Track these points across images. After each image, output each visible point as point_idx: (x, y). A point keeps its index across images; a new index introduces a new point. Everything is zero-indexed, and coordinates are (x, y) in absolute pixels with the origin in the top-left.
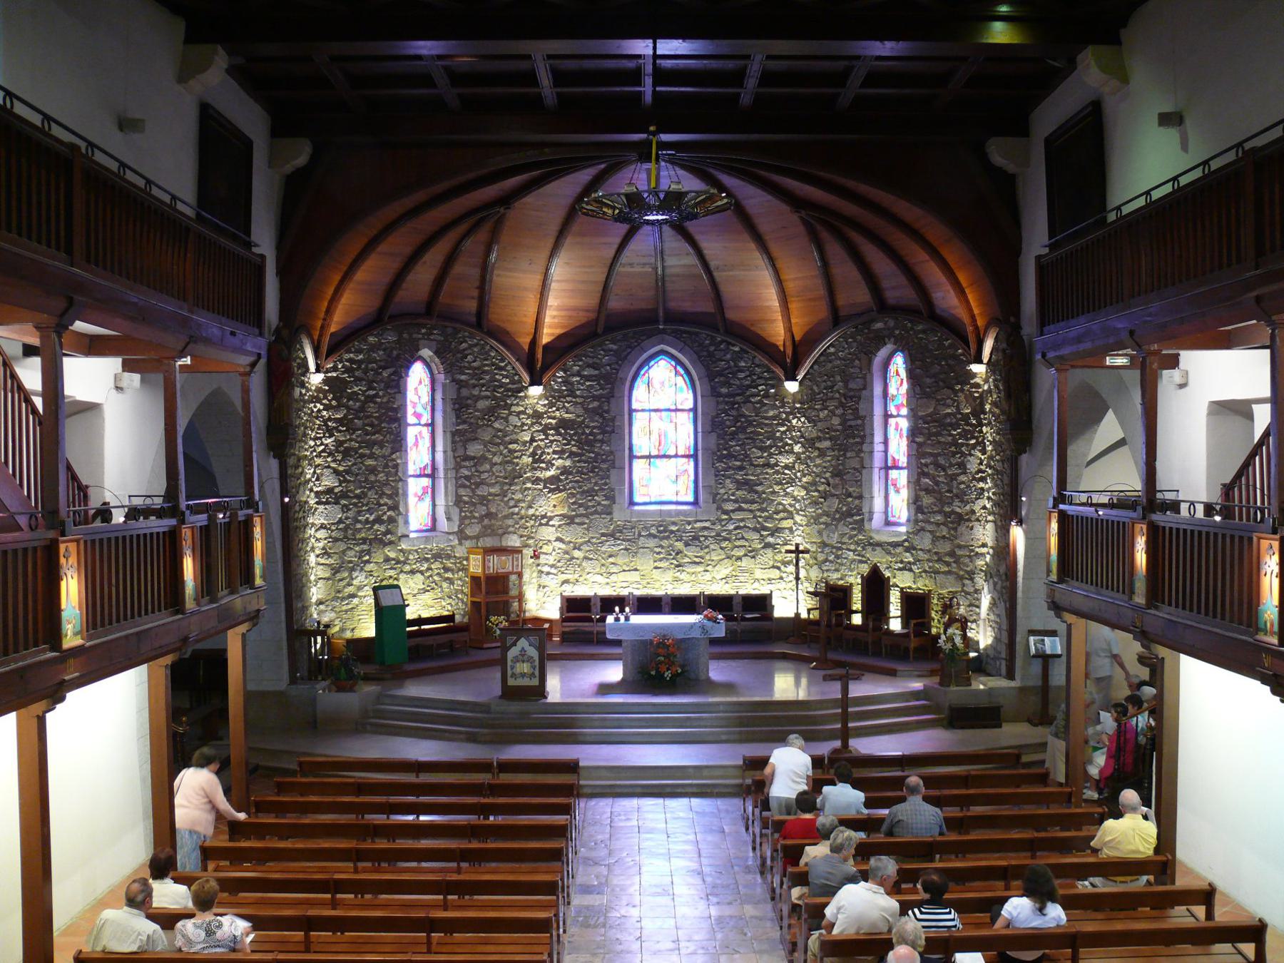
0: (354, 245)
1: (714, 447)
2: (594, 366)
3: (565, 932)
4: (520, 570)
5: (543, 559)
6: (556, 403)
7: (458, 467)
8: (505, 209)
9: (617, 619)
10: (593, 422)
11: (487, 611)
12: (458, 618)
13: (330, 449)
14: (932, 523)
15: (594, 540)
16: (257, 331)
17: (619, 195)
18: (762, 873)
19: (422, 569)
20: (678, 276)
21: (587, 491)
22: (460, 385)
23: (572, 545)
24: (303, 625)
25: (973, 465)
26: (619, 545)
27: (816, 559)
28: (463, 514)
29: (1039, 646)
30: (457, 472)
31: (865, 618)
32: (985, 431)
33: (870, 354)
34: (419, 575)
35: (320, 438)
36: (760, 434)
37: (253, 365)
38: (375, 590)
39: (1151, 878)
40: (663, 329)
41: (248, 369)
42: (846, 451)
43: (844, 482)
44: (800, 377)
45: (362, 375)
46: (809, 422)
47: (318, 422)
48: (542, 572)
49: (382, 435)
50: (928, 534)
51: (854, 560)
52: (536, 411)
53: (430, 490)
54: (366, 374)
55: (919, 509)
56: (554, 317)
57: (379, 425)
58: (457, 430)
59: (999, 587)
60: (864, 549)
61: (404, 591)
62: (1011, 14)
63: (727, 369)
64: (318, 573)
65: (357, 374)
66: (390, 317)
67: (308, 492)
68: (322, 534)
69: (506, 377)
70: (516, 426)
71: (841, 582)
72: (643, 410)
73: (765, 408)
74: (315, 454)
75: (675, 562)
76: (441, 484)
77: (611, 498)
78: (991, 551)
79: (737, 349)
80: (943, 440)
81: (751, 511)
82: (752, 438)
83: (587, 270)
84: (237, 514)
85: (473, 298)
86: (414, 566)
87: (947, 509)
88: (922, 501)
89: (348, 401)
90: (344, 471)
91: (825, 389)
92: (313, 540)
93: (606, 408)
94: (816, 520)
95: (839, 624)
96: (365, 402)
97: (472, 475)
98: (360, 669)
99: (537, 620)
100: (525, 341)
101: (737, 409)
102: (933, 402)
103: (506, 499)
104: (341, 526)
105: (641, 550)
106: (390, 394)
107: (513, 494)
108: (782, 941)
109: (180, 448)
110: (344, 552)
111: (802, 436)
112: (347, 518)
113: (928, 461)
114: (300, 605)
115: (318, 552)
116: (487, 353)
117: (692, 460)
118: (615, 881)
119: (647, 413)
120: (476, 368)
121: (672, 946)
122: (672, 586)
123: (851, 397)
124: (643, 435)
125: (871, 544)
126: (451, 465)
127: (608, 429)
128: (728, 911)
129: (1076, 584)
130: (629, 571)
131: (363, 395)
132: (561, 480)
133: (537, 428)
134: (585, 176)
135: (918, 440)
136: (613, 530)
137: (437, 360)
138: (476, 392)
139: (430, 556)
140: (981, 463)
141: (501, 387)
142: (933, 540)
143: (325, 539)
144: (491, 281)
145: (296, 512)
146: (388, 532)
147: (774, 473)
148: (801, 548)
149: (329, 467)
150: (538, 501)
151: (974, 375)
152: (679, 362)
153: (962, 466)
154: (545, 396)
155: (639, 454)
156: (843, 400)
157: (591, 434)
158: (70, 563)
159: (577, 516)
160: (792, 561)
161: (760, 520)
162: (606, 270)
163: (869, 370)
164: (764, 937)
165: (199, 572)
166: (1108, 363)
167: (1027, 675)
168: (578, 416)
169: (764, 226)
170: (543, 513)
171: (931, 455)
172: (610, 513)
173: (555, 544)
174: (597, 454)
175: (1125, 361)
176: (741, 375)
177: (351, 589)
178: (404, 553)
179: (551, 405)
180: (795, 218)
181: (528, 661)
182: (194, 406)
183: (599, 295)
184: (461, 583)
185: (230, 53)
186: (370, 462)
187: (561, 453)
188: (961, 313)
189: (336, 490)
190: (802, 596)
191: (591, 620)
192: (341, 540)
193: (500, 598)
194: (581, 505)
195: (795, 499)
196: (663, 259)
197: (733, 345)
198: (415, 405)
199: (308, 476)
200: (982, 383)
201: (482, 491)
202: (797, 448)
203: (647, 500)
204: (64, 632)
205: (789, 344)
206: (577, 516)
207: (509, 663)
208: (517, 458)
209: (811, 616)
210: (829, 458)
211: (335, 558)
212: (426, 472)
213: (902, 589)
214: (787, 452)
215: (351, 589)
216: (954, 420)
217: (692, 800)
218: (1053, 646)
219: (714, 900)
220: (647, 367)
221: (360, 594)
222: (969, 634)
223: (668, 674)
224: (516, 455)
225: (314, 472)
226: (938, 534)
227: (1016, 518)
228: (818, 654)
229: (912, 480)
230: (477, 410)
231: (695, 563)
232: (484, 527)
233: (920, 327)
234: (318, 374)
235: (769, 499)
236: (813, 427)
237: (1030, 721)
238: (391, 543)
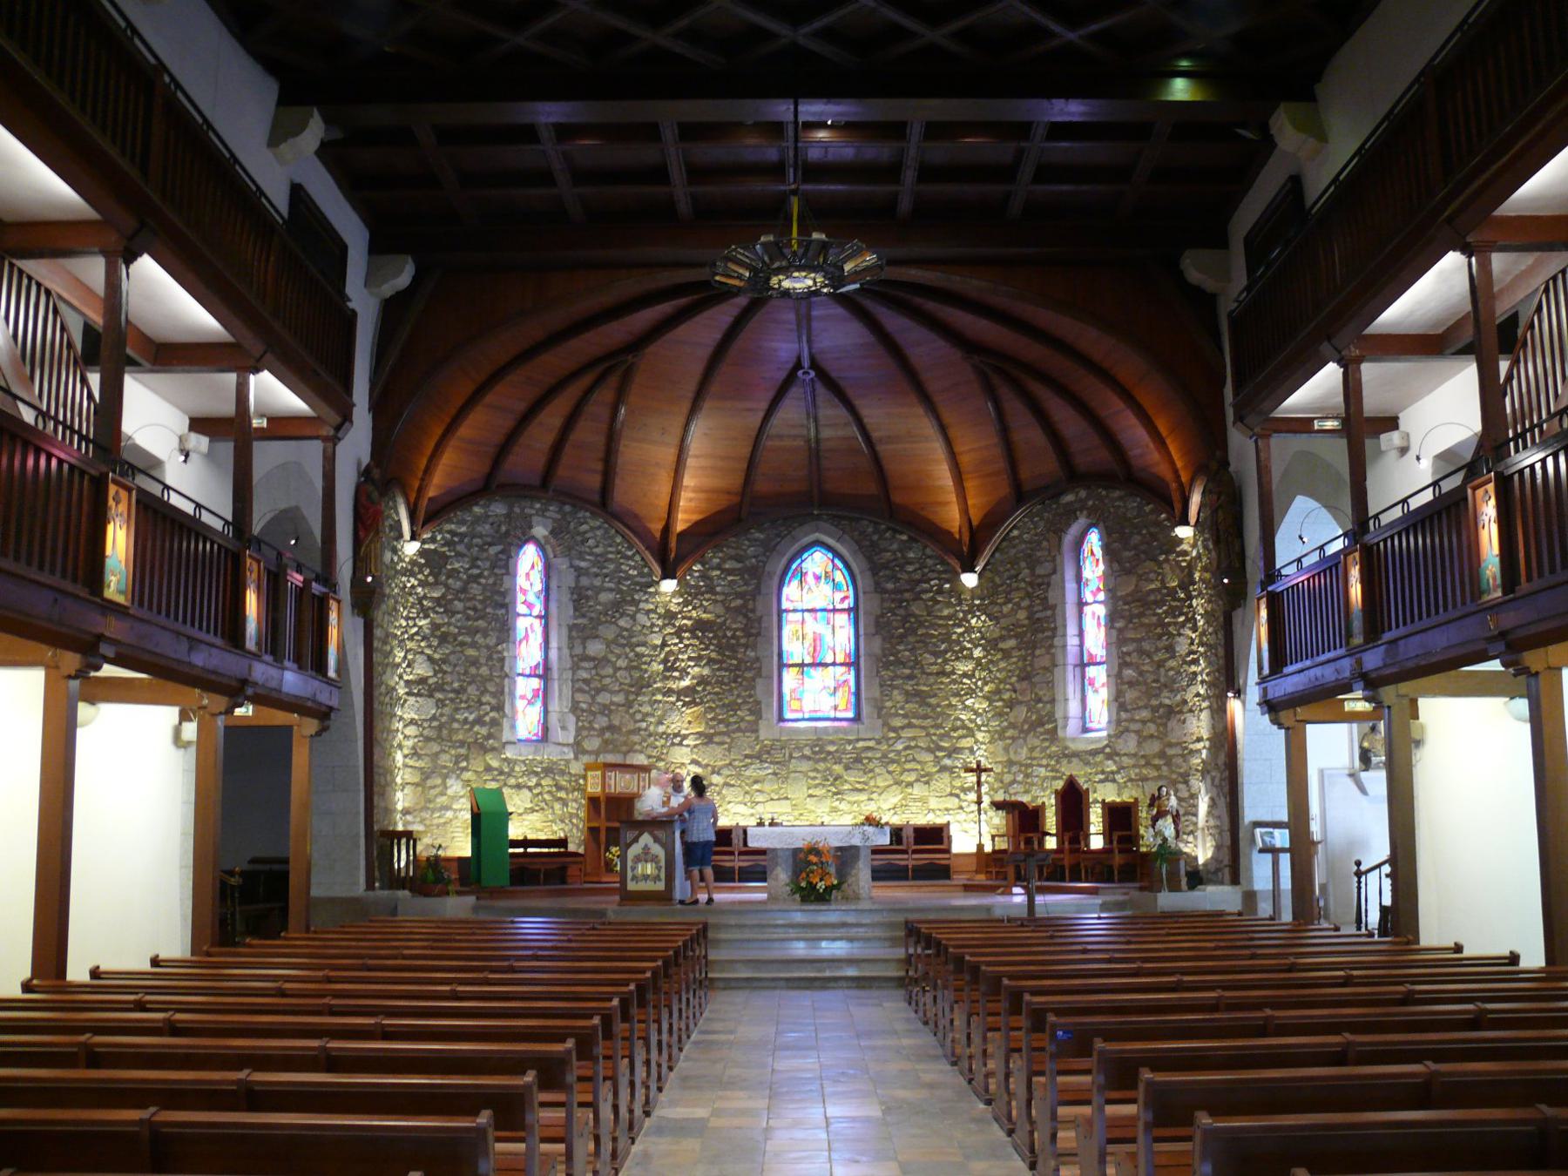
1: (878, 651)
2: (738, 559)
7: (575, 668)
8: (634, 357)
10: (735, 622)
14: (1137, 721)
15: (736, 763)
19: (530, 784)
21: (729, 705)
22: (580, 572)
25: (1182, 647)
27: (1002, 782)
28: (580, 724)
29: (1267, 839)
30: (573, 674)
31: (1060, 842)
32: (1195, 605)
33: (1059, 532)
34: (526, 792)
35: (414, 619)
36: (933, 636)
42: (1035, 648)
44: (978, 569)
46: (991, 620)
50: (1133, 735)
51: (1047, 777)
52: (668, 611)
54: (469, 550)
56: (691, 500)
60: (1058, 762)
62: (1196, 69)
64: (406, 777)
66: (498, 486)
68: (412, 730)
72: (795, 611)
75: (834, 790)
77: (757, 712)
79: (904, 537)
80: (1147, 621)
82: (924, 641)
86: (520, 780)
87: (1154, 702)
89: (448, 578)
90: (440, 659)
91: (1008, 579)
94: (1000, 735)
96: (467, 583)
97: (592, 678)
100: (656, 527)
103: (631, 711)
104: (435, 724)
105: (793, 775)
106: (496, 575)
110: (437, 755)
111: (982, 638)
112: (442, 715)
115: (406, 751)
116: (612, 538)
117: (852, 668)
123: (1039, 585)
130: (779, 799)
133: (669, 630)
135: (1118, 625)
136: (760, 752)
138: (597, 582)
139: (539, 770)
140: (1192, 644)
141: (627, 579)
143: (416, 737)
145: (381, 694)
146: (490, 736)
147: (950, 683)
149: (422, 653)
151: (1181, 541)
152: (837, 554)
153: (1170, 649)
156: (1030, 589)
157: (733, 637)
158: (120, 510)
160: (973, 787)
161: (934, 738)
163: (1059, 551)
166: (1316, 427)
168: (719, 617)
169: (933, 386)
170: (676, 731)
171: (1133, 640)
172: (756, 731)
174: (740, 661)
175: (1336, 423)
176: (910, 568)
177: (442, 800)
178: (509, 764)
179: (686, 603)
184: (576, 807)
185: (327, 120)
186: (471, 652)
187: (698, 659)
188: (1163, 470)
189: (431, 681)
192: (434, 740)
194: (721, 722)
195: (976, 713)
197: (901, 533)
198: (524, 592)
199: (398, 660)
201: (604, 698)
202: (977, 653)
203: (799, 716)
204: (107, 582)
207: (629, 864)
208: (645, 663)
210: (1014, 660)
214: (965, 657)
215: (442, 800)
216: (1159, 597)
221: (455, 807)
223: (821, 886)
224: (644, 659)
225: (405, 657)
226: (1145, 734)
230: (599, 604)
235: (945, 713)
238: (493, 749)
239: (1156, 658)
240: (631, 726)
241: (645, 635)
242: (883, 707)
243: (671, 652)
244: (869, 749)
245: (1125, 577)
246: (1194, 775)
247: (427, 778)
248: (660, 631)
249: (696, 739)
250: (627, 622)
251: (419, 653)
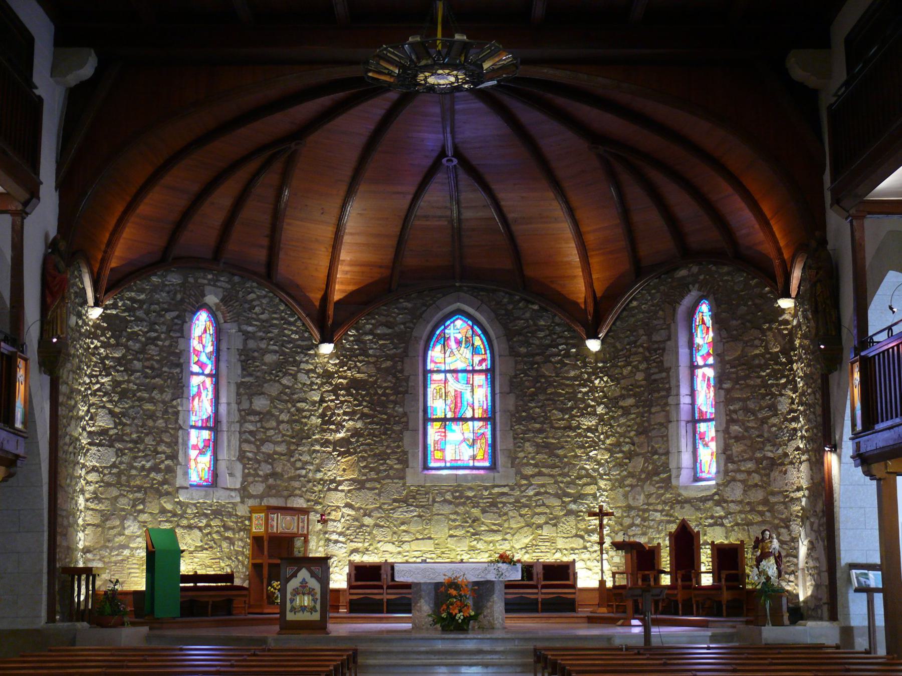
2: (388, 325)
4: (305, 532)
5: (331, 526)
6: (347, 363)
7: (242, 421)
10: (385, 381)
13: (106, 388)
15: (386, 506)
19: (200, 525)
21: (379, 455)
22: (247, 336)
23: (362, 511)
25: (784, 405)
26: (411, 511)
28: (246, 471)
30: (241, 426)
32: (795, 368)
33: (674, 303)
34: (197, 532)
35: (96, 376)
36: (561, 395)
40: (460, 287)
42: (651, 406)
45: (144, 316)
46: (612, 381)
47: (95, 359)
48: (330, 540)
49: (162, 379)
50: (739, 484)
51: (662, 521)
52: (326, 371)
55: (729, 459)
56: (347, 272)
58: (243, 382)
59: (815, 526)
60: (672, 508)
63: (526, 327)
67: (80, 430)
69: (296, 332)
70: (305, 384)
73: (566, 368)
74: (89, 392)
75: (472, 531)
79: (536, 307)
86: (192, 521)
87: (758, 455)
88: (731, 450)
89: (128, 341)
90: (120, 413)
91: (628, 344)
92: (83, 482)
93: (399, 368)
94: (619, 483)
96: (145, 345)
103: (292, 460)
104: (115, 471)
105: (436, 517)
106: (172, 338)
110: (116, 498)
111: (605, 397)
112: (121, 463)
115: (88, 496)
116: (276, 306)
122: (469, 556)
123: (656, 350)
127: (401, 389)
130: (423, 539)
131: (143, 336)
132: (351, 443)
135: (725, 386)
138: (263, 345)
139: (209, 512)
140: (793, 403)
141: (289, 342)
142: (744, 491)
143: (97, 483)
146: (165, 482)
147: (576, 436)
149: (104, 407)
150: (326, 465)
151: (783, 311)
152: (476, 322)
153: (773, 408)
156: (647, 354)
157: (384, 394)
159: (368, 480)
161: (562, 485)
163: (673, 320)
171: (739, 399)
173: (344, 510)
174: (390, 416)
176: (541, 334)
177: (120, 539)
179: (342, 364)
181: (309, 594)
184: (242, 545)
186: (149, 406)
187: (351, 414)
188: (767, 248)
189: (111, 432)
192: (114, 485)
194: (372, 469)
195: (599, 463)
197: (533, 303)
198: (198, 353)
199: (81, 413)
201: (268, 448)
202: (600, 410)
206: (368, 480)
207: (289, 596)
208: (305, 417)
210: (633, 416)
211: (106, 504)
212: (208, 425)
214: (589, 414)
215: (120, 539)
216: (763, 361)
223: (460, 616)
224: (304, 414)
225: (88, 411)
226: (750, 483)
227: (830, 444)
230: (265, 364)
232: (270, 487)
235: (571, 464)
236: (616, 385)
238: (168, 494)
240: (292, 473)
241: (305, 392)
243: (328, 407)
246: (794, 520)
247: (107, 520)
248: (318, 389)
251: (101, 407)
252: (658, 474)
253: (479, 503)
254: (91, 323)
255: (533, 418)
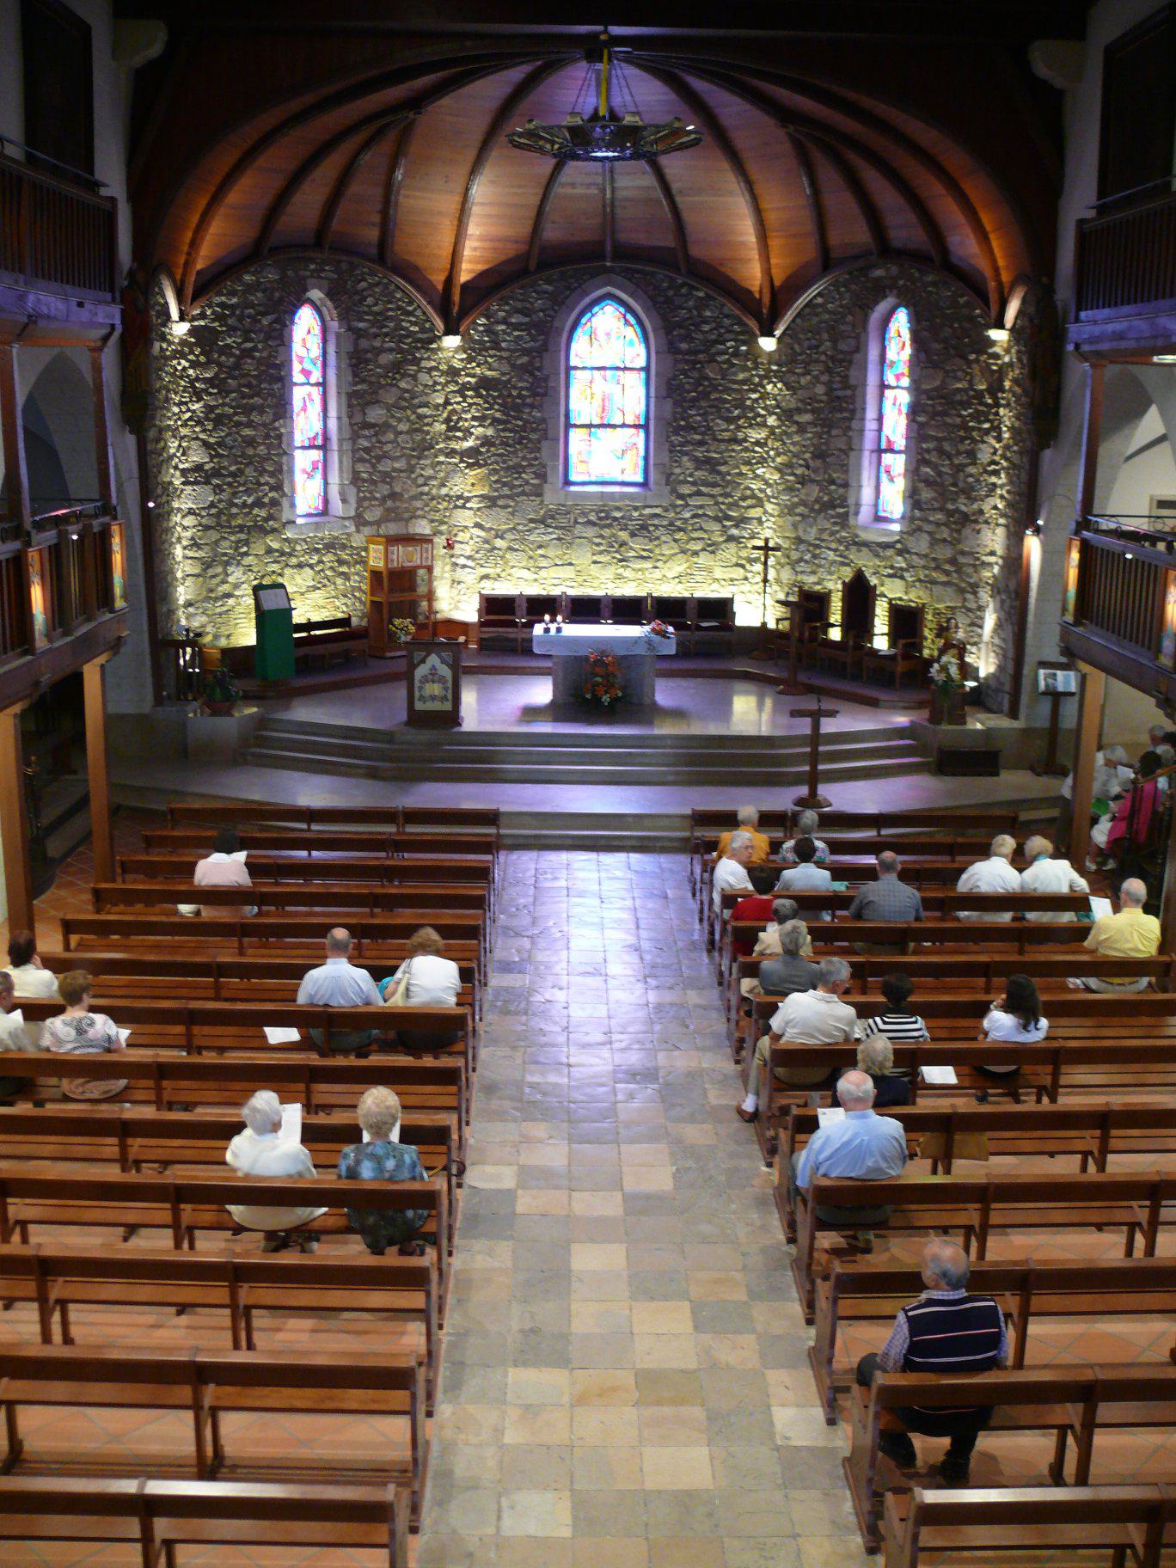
0: (224, 158)
3: (481, 1020)
5: (458, 549)
7: (355, 437)
9: (547, 630)
11: (390, 612)
12: (355, 621)
14: (931, 522)
15: (520, 527)
16: (108, 296)
17: (560, 127)
18: (709, 951)
19: (312, 561)
20: (631, 200)
21: (513, 467)
22: (358, 334)
24: (169, 633)
25: (984, 456)
29: (1050, 681)
31: (845, 633)
33: (867, 307)
34: (307, 569)
35: (186, 403)
36: (726, 401)
37: (106, 339)
38: (257, 590)
39: (1153, 979)
40: (612, 267)
41: (99, 344)
42: (830, 427)
43: (827, 466)
44: (778, 333)
45: (237, 324)
46: (788, 389)
50: (926, 536)
51: (835, 562)
52: (451, 368)
53: (320, 465)
56: (475, 249)
57: (259, 386)
61: (289, 589)
65: (230, 321)
66: (271, 250)
67: (172, 471)
68: (189, 521)
69: (415, 324)
71: (817, 588)
72: (584, 368)
76: (334, 458)
77: (542, 477)
78: (1000, 561)
81: (712, 496)
82: (717, 406)
83: (516, 190)
84: (91, 525)
85: (374, 225)
87: (950, 506)
90: (216, 443)
92: (179, 529)
93: (538, 365)
94: (789, 510)
95: (813, 638)
96: (240, 358)
97: (373, 447)
98: (237, 686)
99: (450, 623)
100: (438, 279)
101: (699, 370)
102: (941, 374)
103: (413, 476)
104: (213, 511)
105: (578, 540)
107: (422, 469)
108: (729, 1036)
109: (19, 422)
110: (216, 543)
111: (778, 406)
112: (220, 501)
113: (931, 445)
114: (165, 609)
115: (185, 543)
116: (391, 294)
118: (540, 957)
119: (588, 372)
120: (377, 314)
121: (600, 1038)
124: (583, 399)
125: (856, 543)
126: (347, 435)
128: (669, 997)
129: (1093, 627)
132: (481, 453)
133: (452, 387)
134: (517, 74)
135: (921, 419)
137: (329, 303)
138: (377, 343)
141: (407, 336)
144: (396, 203)
146: (270, 517)
148: (771, 544)
149: (197, 438)
151: (993, 343)
152: (629, 309)
153: (972, 455)
154: (463, 349)
155: (578, 423)
159: (501, 497)
160: (759, 559)
161: (723, 507)
162: (541, 191)
164: (709, 1031)
165: (49, 605)
167: (1036, 715)
168: (503, 374)
169: (741, 140)
172: (540, 495)
174: (526, 422)
176: (706, 328)
179: (470, 359)
180: (781, 133)
182: (33, 379)
183: (531, 222)
184: (359, 580)
186: (247, 432)
187: (481, 419)
188: (982, 264)
189: (207, 467)
190: (770, 602)
191: (514, 624)
192: (213, 528)
193: (407, 596)
194: (505, 484)
195: (766, 483)
196: (613, 180)
197: (698, 290)
198: (301, 360)
199: (172, 451)
200: (1002, 353)
202: (771, 421)
205: (766, 291)
206: (501, 497)
207: (417, 684)
208: (428, 424)
209: (780, 627)
210: (810, 435)
213: (891, 600)
214: (758, 424)
215: (225, 588)
217: (631, 855)
218: (1067, 682)
219: (652, 982)
220: (589, 315)
221: (236, 593)
222: (968, 659)
223: (606, 699)
224: (426, 421)
225: (180, 446)
226: (937, 537)
228: (784, 675)
229: (911, 468)
230: (379, 366)
231: (643, 557)
232: (388, 510)
233: (930, 278)
234: (182, 324)
236: (792, 395)
237: (1032, 769)
238: (274, 530)
239: (956, 462)
240: (414, 491)
241: (426, 394)
242: (672, 474)
243: (454, 411)
244: (656, 516)
245: (932, 371)
247: (208, 568)
249: (480, 502)
250: (407, 382)
251: (194, 439)
252: (834, 507)
253: (626, 525)
254: (176, 341)
255: (694, 428)
